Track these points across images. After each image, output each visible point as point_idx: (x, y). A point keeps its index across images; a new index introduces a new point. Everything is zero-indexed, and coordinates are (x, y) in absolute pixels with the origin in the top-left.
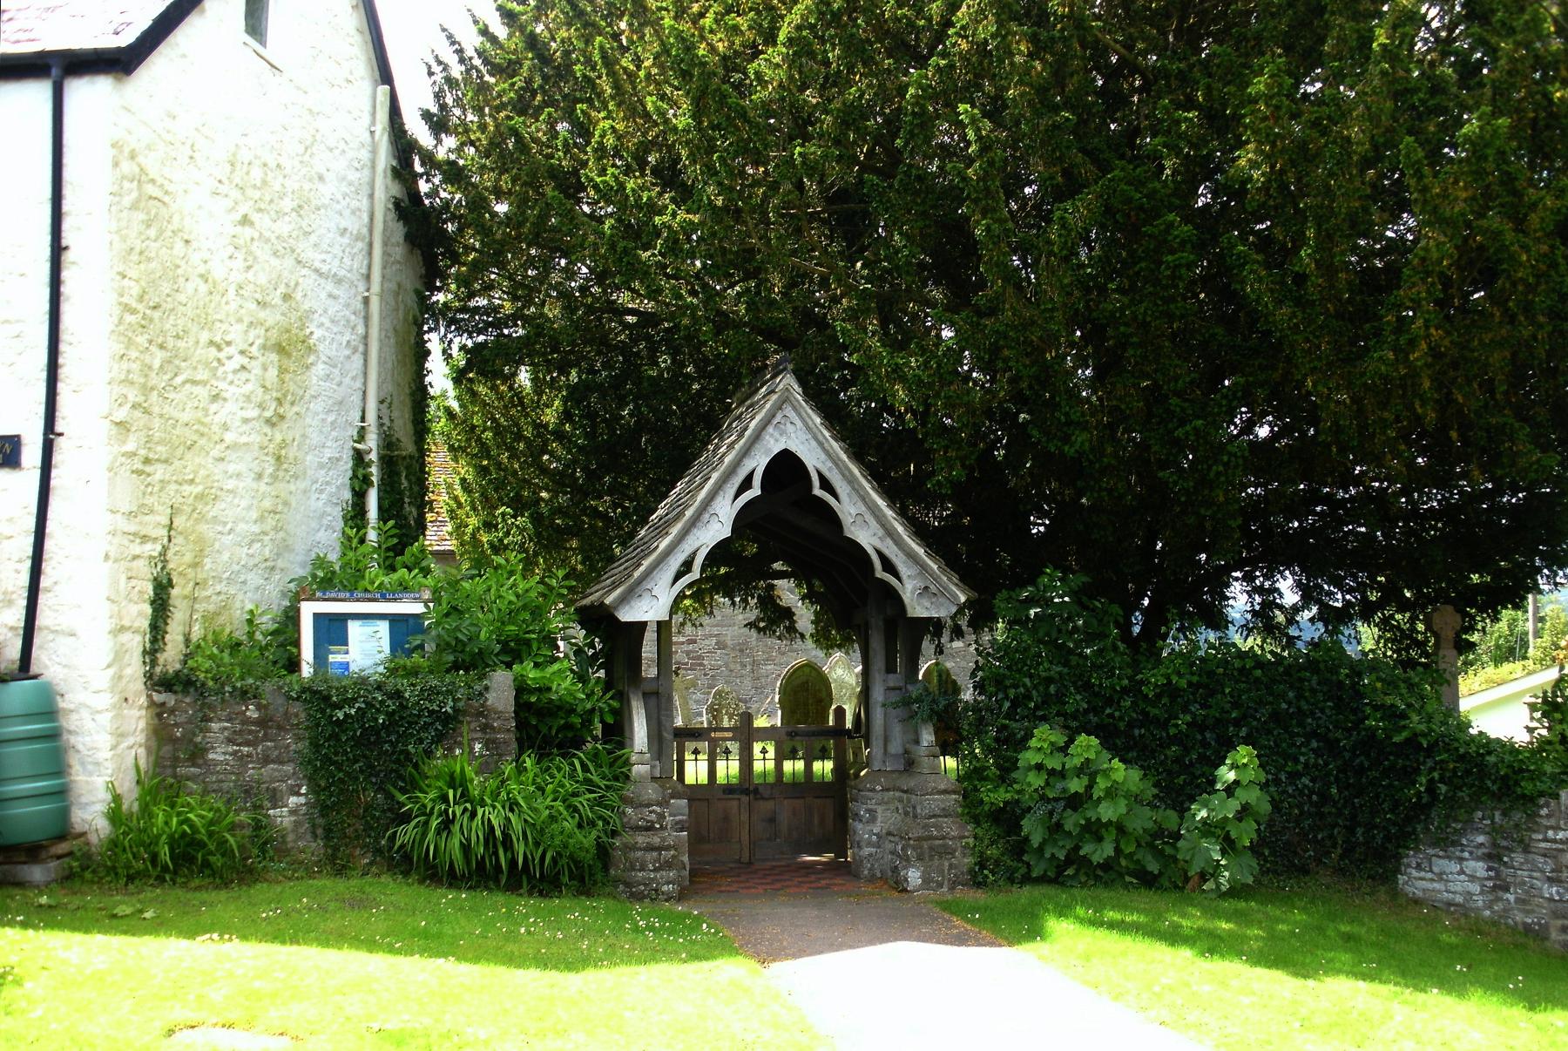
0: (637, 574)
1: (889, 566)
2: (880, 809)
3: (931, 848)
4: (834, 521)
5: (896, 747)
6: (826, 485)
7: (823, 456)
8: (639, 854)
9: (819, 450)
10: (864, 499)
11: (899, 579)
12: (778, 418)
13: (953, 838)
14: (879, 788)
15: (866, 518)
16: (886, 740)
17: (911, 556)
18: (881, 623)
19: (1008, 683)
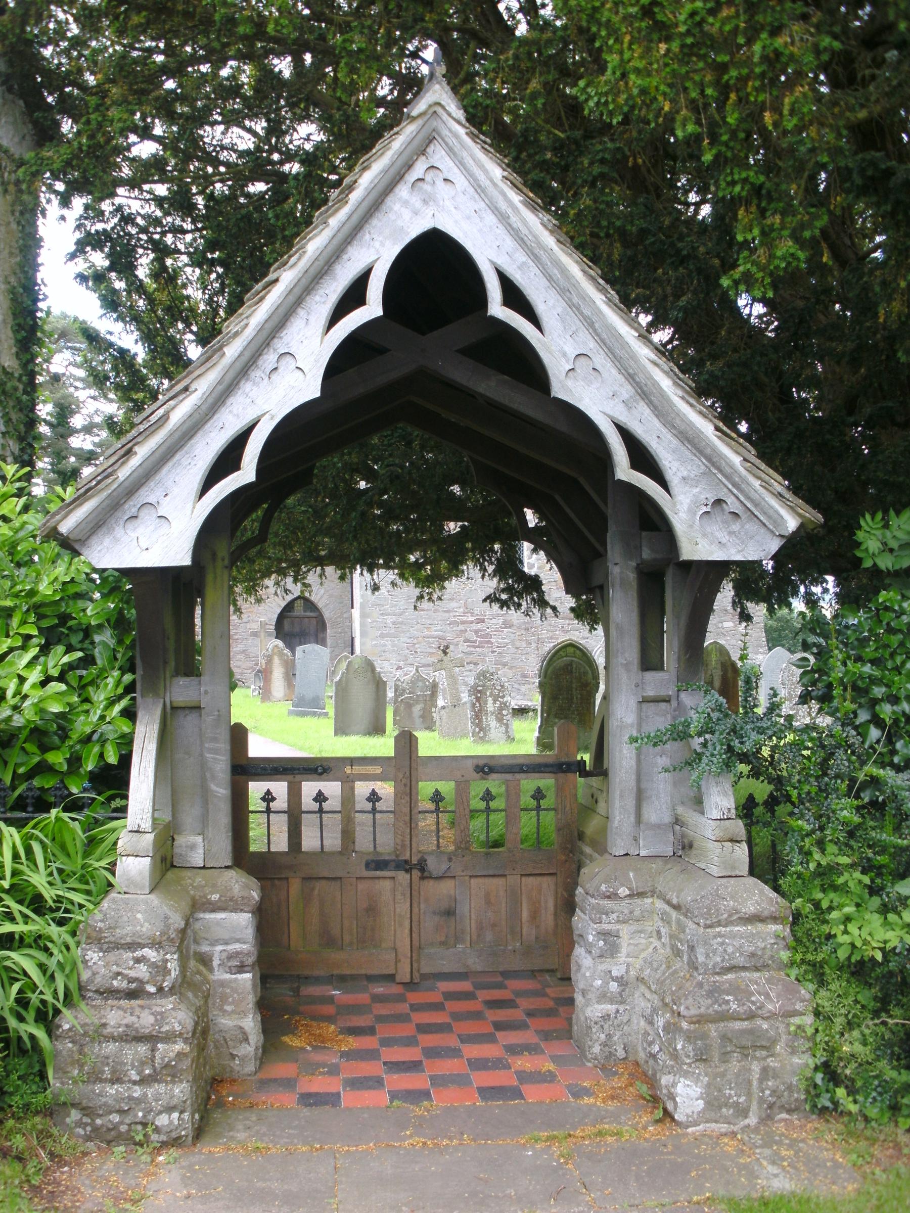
0: (124, 473)
1: (642, 458)
2: (625, 931)
3: (725, 1038)
4: (528, 368)
5: (657, 812)
6: (514, 297)
7: (509, 243)
8: (110, 1048)
9: (501, 231)
10: (591, 324)
11: (663, 483)
12: (419, 169)
13: (771, 1016)
14: (623, 891)
15: (601, 360)
16: (640, 797)
17: (688, 438)
18: (632, 576)
19: (878, 691)
